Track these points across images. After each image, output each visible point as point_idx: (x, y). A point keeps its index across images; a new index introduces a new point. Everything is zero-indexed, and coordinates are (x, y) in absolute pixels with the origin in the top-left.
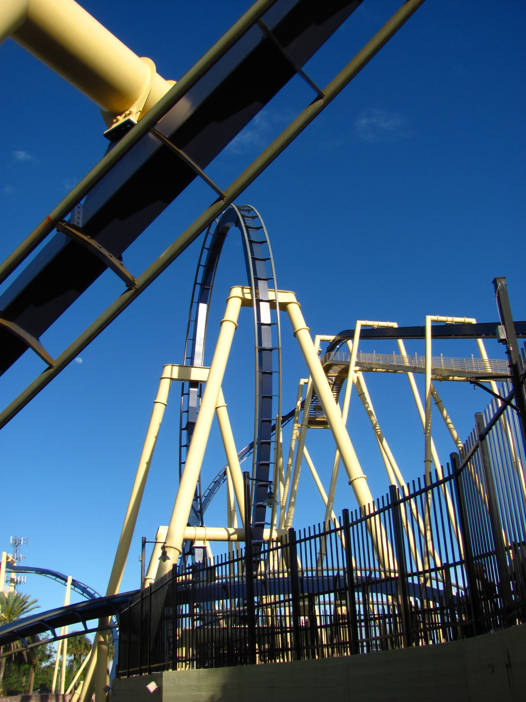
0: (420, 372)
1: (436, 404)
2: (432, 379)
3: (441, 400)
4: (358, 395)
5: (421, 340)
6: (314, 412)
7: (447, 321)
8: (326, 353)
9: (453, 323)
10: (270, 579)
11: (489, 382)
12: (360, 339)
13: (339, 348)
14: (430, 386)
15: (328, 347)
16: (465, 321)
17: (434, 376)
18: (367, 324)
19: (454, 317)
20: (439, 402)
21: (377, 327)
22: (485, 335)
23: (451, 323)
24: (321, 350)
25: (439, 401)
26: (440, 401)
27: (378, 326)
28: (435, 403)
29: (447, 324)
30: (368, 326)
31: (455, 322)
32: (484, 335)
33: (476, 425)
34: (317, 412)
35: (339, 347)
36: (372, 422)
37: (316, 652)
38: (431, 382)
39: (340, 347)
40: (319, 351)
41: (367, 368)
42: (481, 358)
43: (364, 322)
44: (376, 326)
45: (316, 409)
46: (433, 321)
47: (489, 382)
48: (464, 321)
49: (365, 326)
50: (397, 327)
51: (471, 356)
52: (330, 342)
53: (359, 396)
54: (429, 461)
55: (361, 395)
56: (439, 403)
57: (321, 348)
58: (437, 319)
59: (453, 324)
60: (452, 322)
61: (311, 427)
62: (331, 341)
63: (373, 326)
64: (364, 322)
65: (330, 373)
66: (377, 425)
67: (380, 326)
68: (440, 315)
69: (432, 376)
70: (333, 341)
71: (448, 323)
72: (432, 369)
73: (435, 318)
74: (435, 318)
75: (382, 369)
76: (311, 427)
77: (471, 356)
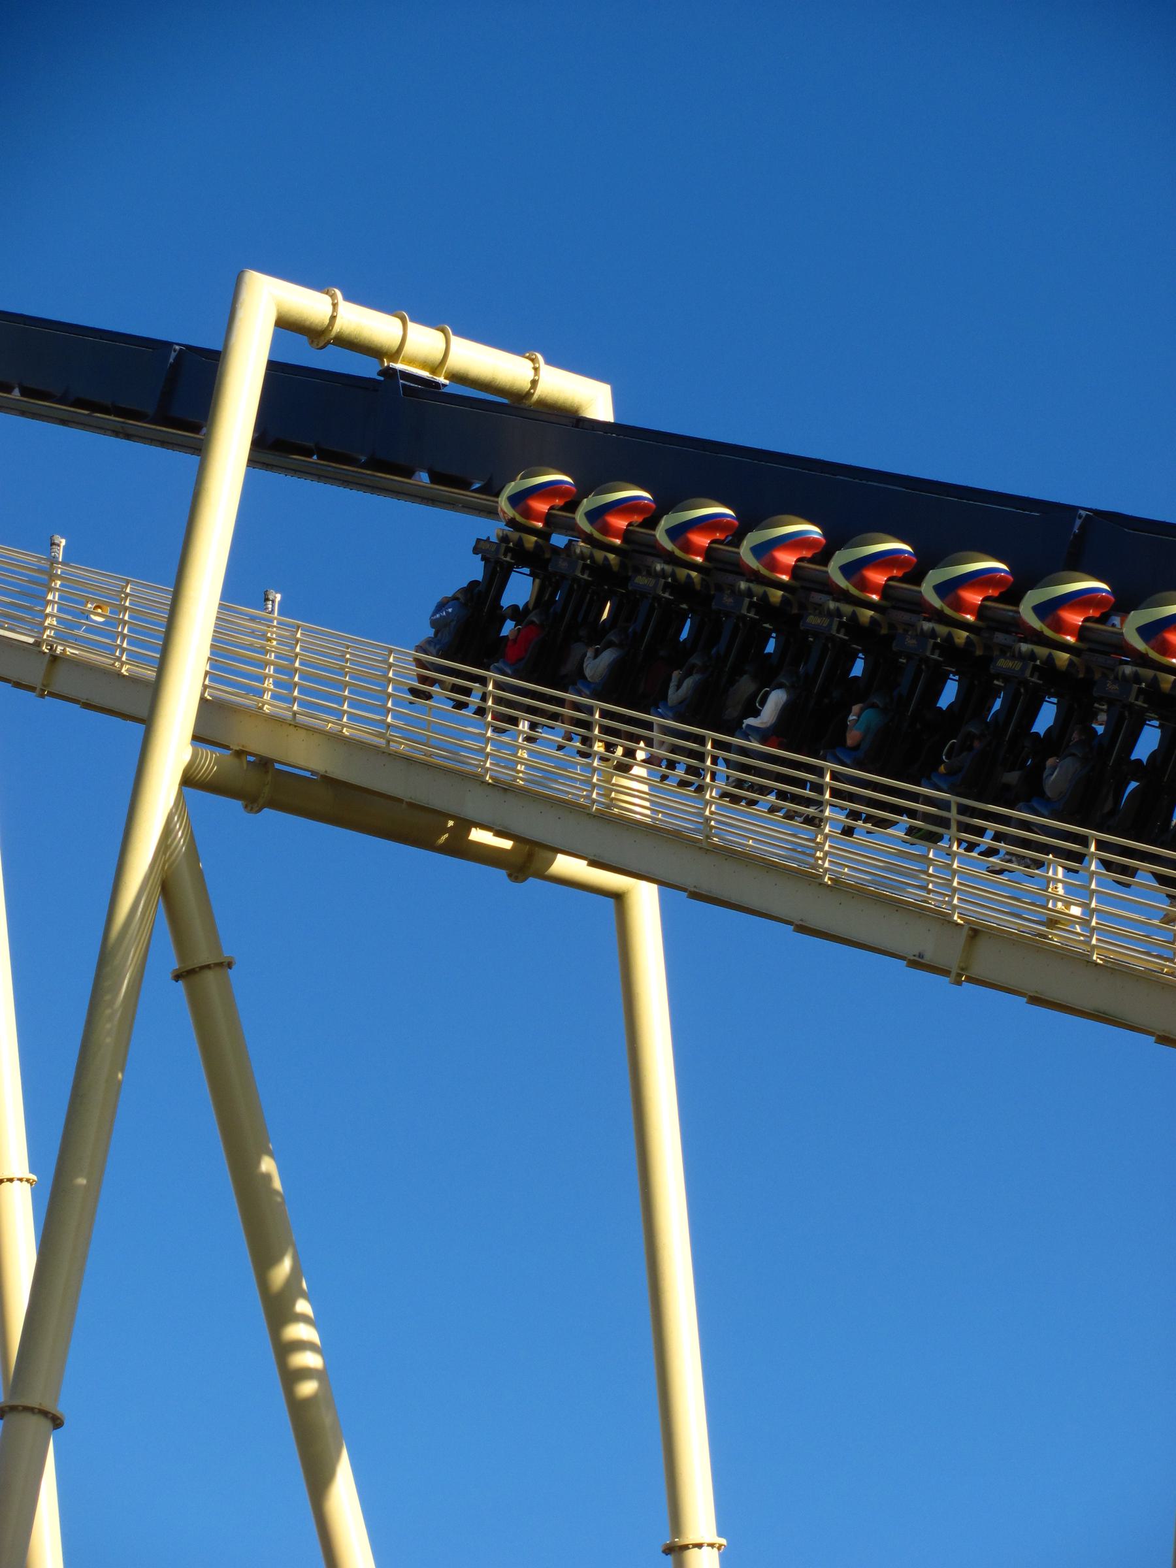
0: (812, 923)
1: (177, 977)
2: (189, 780)
3: (227, 953)
5: (185, 460)
7: (396, 354)
9: (441, 379)
11: (618, 898)
12: (253, 462)
14: (168, 832)
16: (534, 383)
17: (210, 759)
19: (459, 333)
22: (436, 478)
23: (425, 374)
25: (204, 956)
26: (220, 965)
28: (175, 965)
29: (390, 373)
31: (459, 378)
32: (424, 477)
33: (121, 1063)
38: (180, 793)
46: (286, 325)
47: (618, 898)
48: (527, 385)
49: (315, 335)
50: (612, 420)
51: (267, 599)
54: (44, 1413)
56: (210, 975)
59: (437, 385)
60: (434, 370)
68: (358, 296)
69: (195, 756)
71: (399, 366)
72: (203, 700)
75: (594, 863)
77: (267, 599)
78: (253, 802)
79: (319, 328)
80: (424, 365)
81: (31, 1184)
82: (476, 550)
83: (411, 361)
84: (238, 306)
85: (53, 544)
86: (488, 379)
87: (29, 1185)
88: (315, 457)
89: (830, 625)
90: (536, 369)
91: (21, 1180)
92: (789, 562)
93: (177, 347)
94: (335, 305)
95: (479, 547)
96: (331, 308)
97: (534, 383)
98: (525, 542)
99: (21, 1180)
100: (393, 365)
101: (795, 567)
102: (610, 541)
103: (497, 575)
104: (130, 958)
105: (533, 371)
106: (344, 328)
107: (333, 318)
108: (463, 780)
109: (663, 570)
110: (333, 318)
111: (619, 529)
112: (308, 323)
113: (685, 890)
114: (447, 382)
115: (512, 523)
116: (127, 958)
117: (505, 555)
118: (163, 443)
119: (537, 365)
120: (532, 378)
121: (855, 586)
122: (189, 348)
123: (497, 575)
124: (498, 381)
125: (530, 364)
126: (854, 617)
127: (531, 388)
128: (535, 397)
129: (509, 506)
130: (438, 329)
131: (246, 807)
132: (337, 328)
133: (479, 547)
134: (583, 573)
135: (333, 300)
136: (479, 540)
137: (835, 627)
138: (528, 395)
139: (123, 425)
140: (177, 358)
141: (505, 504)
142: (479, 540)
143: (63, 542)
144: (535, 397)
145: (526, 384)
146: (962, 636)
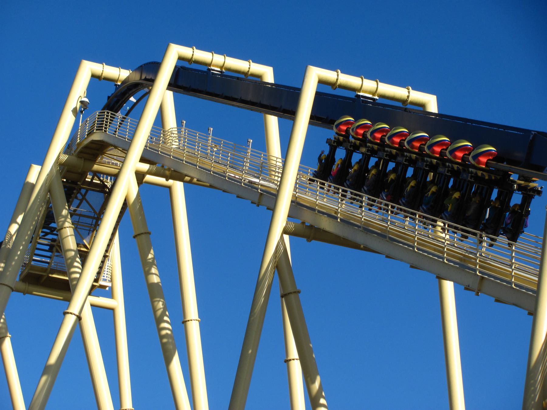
4: (134, 234)
5: (290, 122)
6: (49, 254)
7: (360, 90)
8: (104, 109)
9: (376, 97)
10: (487, 164)
12: (310, 123)
13: (135, 104)
15: (110, 95)
16: (408, 97)
18: (194, 57)
20: (291, 293)
21: (219, 69)
23: (370, 96)
24: (86, 100)
25: (290, 289)
26: (295, 292)
27: (221, 67)
30: (197, 62)
31: (382, 96)
34: (57, 256)
35: (135, 101)
36: (155, 310)
37: (439, 254)
39: (138, 101)
40: (82, 102)
41: (169, 169)
42: (266, 152)
43: (187, 52)
44: (217, 66)
45: (54, 249)
49: (333, 85)
52: (116, 85)
53: (134, 237)
55: (139, 235)
57: (87, 97)
58: (247, 69)
60: (374, 94)
61: (35, 293)
62: (119, 83)
63: (210, 65)
64: (187, 52)
65: (100, 164)
66: (166, 318)
67: (229, 70)
69: (287, 224)
70: (124, 82)
71: (361, 94)
73: (330, 75)
74: (330, 75)
76: (35, 293)
78: (309, 239)
79: (333, 83)
80: (370, 93)
81: (199, 322)
82: (327, 142)
83: (365, 92)
84: (305, 77)
85: (182, 122)
86: (392, 96)
87: (198, 322)
88: (505, 163)
89: (445, 171)
90: (409, 92)
91: (196, 320)
92: (484, 161)
93: (533, 133)
94: (338, 75)
95: (328, 141)
96: (337, 76)
97: (408, 97)
98: (433, 162)
99: (196, 320)
100: (359, 94)
101: (487, 162)
102: (395, 146)
103: (333, 150)
104: (266, 284)
105: (408, 93)
106: (342, 82)
107: (337, 79)
108: (469, 286)
109: (449, 165)
110: (337, 79)
111: (460, 157)
112: (329, 81)
113: (221, 190)
114: (378, 98)
115: (337, 133)
116: (265, 285)
117: (334, 143)
118: (223, 103)
119: (409, 91)
120: (407, 95)
121: (477, 163)
122: (539, 133)
123: (333, 150)
124: (396, 97)
125: (407, 90)
126: (410, 157)
127: (407, 98)
128: (409, 101)
129: (407, 145)
130: (375, 81)
131: (307, 240)
132: (339, 83)
133: (328, 141)
134: (471, 178)
135: (337, 73)
136: (327, 139)
137: (446, 172)
138: (407, 101)
139: (510, 168)
140: (533, 137)
141: (448, 153)
142: (327, 139)
143: (185, 122)
144: (409, 101)
145: (406, 97)
146: (455, 166)
